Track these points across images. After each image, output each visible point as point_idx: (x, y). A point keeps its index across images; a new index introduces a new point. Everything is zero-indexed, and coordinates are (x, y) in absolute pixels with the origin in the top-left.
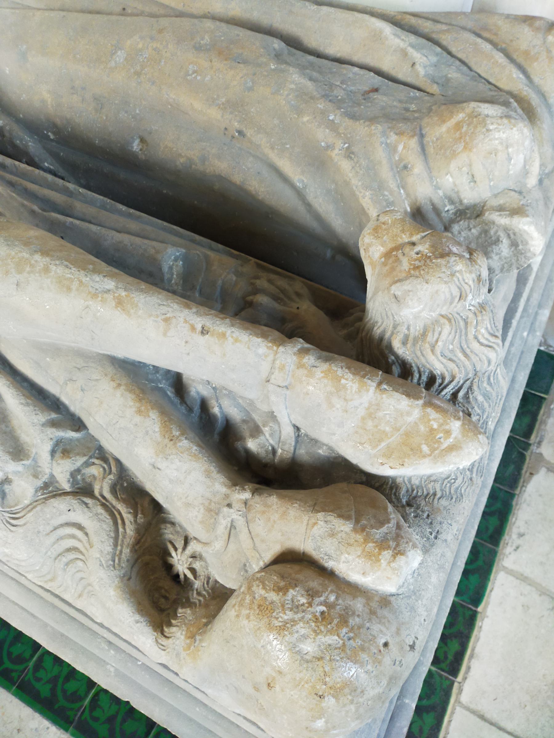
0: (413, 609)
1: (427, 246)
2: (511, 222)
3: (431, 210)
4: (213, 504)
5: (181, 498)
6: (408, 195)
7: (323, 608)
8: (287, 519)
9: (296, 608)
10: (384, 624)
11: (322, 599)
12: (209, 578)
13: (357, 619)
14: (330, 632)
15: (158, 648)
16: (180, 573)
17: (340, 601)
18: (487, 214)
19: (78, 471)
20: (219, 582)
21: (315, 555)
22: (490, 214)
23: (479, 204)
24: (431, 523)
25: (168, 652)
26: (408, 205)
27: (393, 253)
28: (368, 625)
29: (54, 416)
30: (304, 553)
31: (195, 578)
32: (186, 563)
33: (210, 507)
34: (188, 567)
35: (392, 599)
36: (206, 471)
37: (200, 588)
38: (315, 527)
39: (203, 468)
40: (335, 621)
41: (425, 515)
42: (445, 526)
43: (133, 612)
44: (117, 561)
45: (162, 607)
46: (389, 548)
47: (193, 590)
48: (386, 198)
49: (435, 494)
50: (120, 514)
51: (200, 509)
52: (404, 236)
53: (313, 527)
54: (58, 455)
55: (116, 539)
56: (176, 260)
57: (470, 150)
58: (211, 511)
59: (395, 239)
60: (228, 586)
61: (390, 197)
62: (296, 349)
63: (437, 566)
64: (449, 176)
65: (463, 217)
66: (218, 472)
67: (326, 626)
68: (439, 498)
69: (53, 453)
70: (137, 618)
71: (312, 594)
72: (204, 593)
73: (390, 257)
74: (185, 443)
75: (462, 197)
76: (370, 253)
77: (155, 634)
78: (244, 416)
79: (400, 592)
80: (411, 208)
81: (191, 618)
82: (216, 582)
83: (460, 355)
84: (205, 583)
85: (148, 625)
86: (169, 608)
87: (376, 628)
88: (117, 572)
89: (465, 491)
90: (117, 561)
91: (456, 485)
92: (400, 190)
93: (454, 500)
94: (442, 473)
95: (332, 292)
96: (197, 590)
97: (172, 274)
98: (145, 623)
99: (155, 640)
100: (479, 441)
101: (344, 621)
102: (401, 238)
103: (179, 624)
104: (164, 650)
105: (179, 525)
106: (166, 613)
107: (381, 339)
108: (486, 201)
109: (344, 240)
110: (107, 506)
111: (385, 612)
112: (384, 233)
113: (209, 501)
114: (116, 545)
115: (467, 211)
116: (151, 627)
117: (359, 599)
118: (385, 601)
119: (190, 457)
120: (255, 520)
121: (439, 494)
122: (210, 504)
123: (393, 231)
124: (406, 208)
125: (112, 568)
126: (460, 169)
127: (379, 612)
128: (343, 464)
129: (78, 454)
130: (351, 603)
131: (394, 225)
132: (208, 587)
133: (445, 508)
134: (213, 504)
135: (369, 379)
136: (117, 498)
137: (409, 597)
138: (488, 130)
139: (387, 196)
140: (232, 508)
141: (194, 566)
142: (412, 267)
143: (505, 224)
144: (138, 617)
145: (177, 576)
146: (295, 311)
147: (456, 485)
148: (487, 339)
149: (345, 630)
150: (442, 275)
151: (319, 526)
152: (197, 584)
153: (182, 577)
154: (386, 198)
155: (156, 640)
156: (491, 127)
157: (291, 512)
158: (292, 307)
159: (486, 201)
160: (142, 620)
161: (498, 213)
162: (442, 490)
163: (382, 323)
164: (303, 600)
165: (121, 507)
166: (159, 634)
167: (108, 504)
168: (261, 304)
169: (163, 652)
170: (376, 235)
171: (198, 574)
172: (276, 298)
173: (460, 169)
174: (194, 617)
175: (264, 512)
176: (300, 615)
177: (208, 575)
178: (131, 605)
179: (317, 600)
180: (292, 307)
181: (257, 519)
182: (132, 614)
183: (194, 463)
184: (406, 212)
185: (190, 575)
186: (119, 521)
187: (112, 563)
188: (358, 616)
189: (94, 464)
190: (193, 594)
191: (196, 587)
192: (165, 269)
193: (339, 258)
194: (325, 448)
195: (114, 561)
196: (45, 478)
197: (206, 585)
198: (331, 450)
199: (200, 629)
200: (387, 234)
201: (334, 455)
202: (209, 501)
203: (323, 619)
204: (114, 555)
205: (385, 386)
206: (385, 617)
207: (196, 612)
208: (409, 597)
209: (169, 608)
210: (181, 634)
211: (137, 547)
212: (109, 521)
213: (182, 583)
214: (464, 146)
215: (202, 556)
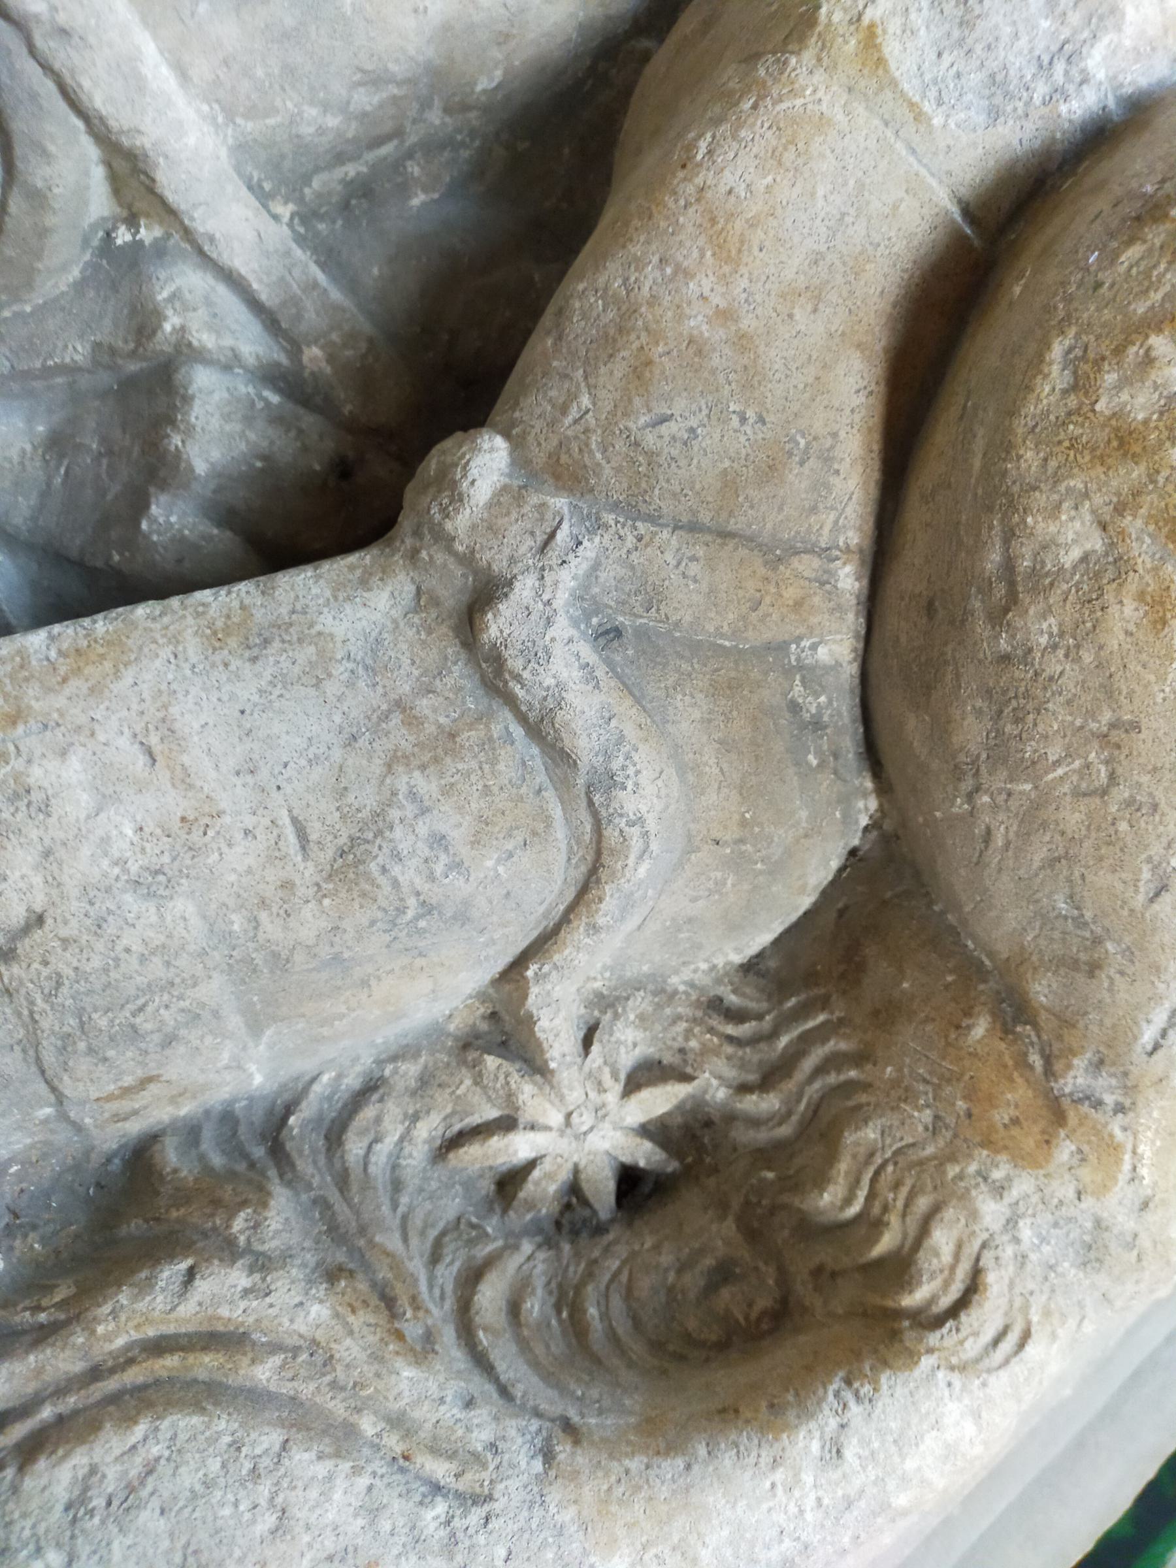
4: (424, 704)
5: (287, 885)
8: (753, 224)
12: (716, 1005)
15: (1003, 1374)
16: (626, 1159)
20: (760, 955)
21: (1014, 135)
25: (1047, 1313)
30: (967, 211)
31: (687, 1078)
32: (601, 1089)
33: (430, 729)
34: (619, 1088)
36: (215, 638)
37: (743, 1065)
38: (891, 48)
43: (775, 1463)
44: (440, 1470)
45: (763, 1302)
47: (731, 1118)
50: (159, 1347)
51: (413, 795)
53: (881, 62)
58: (452, 736)
60: (806, 902)
70: (815, 1446)
72: (784, 1041)
77: (927, 1362)
78: (29, 421)
81: (927, 1116)
82: (750, 967)
84: (730, 1030)
85: (866, 1389)
86: (782, 1271)
90: (440, 1470)
96: (744, 1089)
98: (855, 1409)
99: (956, 1378)
103: (923, 1203)
104: (1026, 1336)
105: (394, 1058)
106: (803, 1289)
110: (60, 1420)
113: (396, 719)
114: (341, 1439)
116: (884, 1378)
119: (76, 685)
120: (651, 455)
122: (413, 721)
125: (476, 1516)
128: (522, 146)
132: (760, 1017)
134: (424, 704)
140: (510, 583)
141: (627, 1060)
144: (806, 1441)
145: (629, 1179)
151: (894, 26)
152: (713, 1085)
153: (644, 1154)
155: (962, 1368)
157: (729, 178)
160: (833, 1423)
166: (933, 1338)
167: (47, 1413)
169: (1030, 1349)
171: (668, 1058)
174: (925, 1094)
175: (641, 371)
177: (698, 1004)
181: (649, 439)
182: (779, 1476)
183: (129, 676)
186: (206, 1364)
187: (441, 1507)
190: (755, 1122)
191: (721, 1094)
194: (414, 169)
195: (437, 1489)
197: (745, 1030)
198: (442, 147)
199: (1023, 1063)
201: (465, 154)
207: (895, 1083)
209: (782, 1271)
210: (999, 1190)
213: (673, 1166)
215: (600, 996)
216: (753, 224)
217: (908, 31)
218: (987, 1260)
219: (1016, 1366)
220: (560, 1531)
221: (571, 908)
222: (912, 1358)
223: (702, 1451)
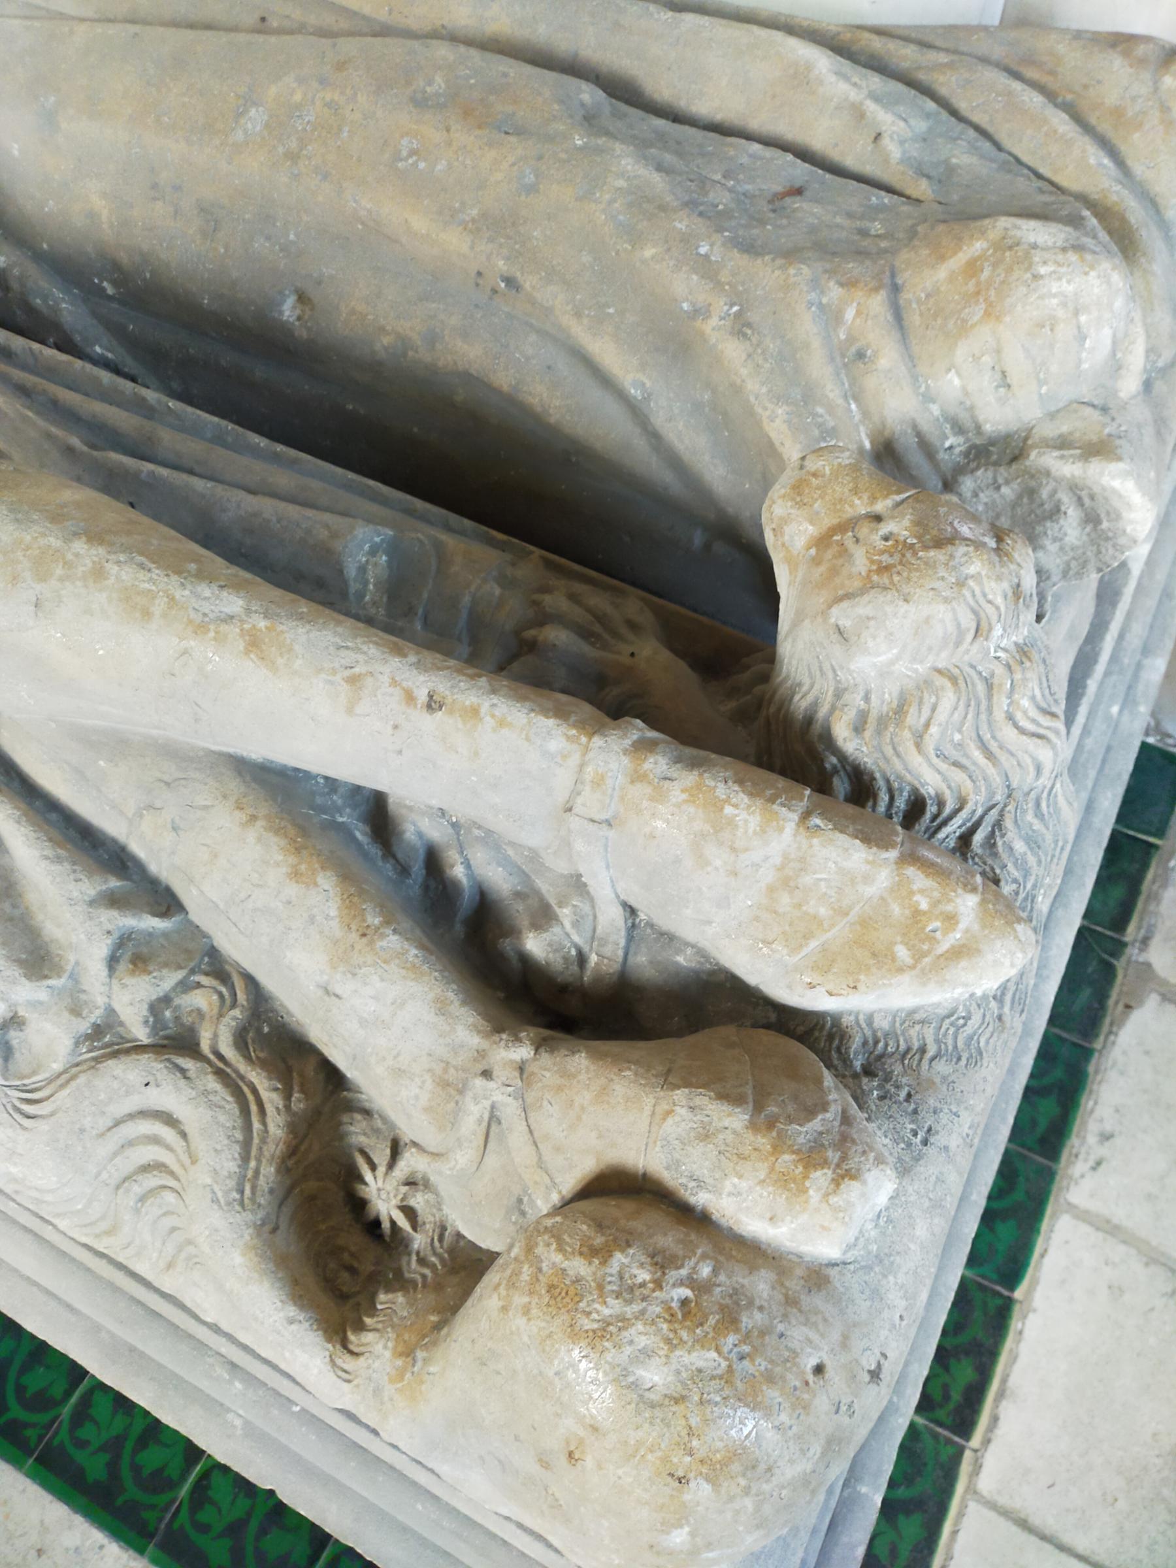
0: (876, 1294)
1: (906, 522)
2: (1085, 472)
3: (915, 445)
4: (452, 1071)
5: (384, 1059)
6: (866, 414)
7: (686, 1292)
8: (608, 1103)
9: (628, 1291)
10: (815, 1325)
11: (684, 1272)
12: (443, 1228)
13: (758, 1316)
14: (701, 1343)
15: (335, 1378)
16: (381, 1218)
17: (722, 1278)
18: (1033, 454)
19: (166, 1000)
20: (464, 1237)
21: (669, 1178)
22: (1040, 454)
23: (1016, 432)
24: (915, 1112)
25: (357, 1386)
26: (867, 435)
27: (835, 538)
28: (781, 1327)
29: (114, 883)
30: (644, 1175)
31: (415, 1228)
32: (395, 1196)
33: (446, 1077)
35: (833, 1272)
36: (437, 1000)
37: (425, 1249)
38: (670, 1121)
39: (431, 995)
40: (712, 1320)
41: (903, 1094)
42: (944, 1117)
43: (282, 1301)
45: (345, 1289)
46: (825, 1163)
48: (820, 420)
49: (923, 1050)
50: (255, 1091)
51: (424, 1082)
52: (857, 502)
53: (664, 1119)
54: (123, 966)
55: (246, 1144)
56: (373, 552)
57: (998, 318)
58: (448, 1085)
59: (838, 507)
61: (828, 418)
62: (627, 742)
63: (927, 1204)
64: (952, 373)
65: (983, 461)
66: (464, 1003)
67: (691, 1330)
68: (933, 1059)
69: (112, 962)
70: (292, 1314)
71: (662, 1262)
72: (433, 1259)
73: (828, 546)
74: (392, 941)
75: (981, 418)
76: (786, 538)
77: (330, 1346)
78: (519, 884)
79: (849, 1257)
80: (872, 443)
81: (405, 1314)
82: (459, 1236)
83: (977, 755)
84: (436, 1238)
86: (359, 1292)
87: (797, 1333)
88: (248, 1216)
89: (987, 1042)
91: (969, 1030)
92: (849, 404)
93: (963, 1062)
94: (938, 1005)
95: (705, 620)
96: (418, 1253)
97: (366, 583)
98: (307, 1324)
99: (328, 1359)
100: (1016, 937)
101: (730, 1319)
102: (851, 506)
103: (380, 1326)
104: (349, 1381)
105: (380, 1116)
106: (352, 1301)
107: (809, 720)
108: (1033, 428)
109: (730, 510)
110: (228, 1074)
111: (817, 1300)
112: (816, 496)
113: (443, 1065)
114: (245, 1158)
115: (991, 448)
116: (320, 1333)
117: (763, 1272)
118: (818, 1277)
120: (541, 1106)
121: (932, 1050)
122: (445, 1071)
123: (834, 490)
124: (861, 441)
125: (238, 1208)
126: (976, 359)
127: (805, 1300)
128: (728, 985)
129: (166, 965)
130: (745, 1282)
131: (837, 479)
132: (442, 1247)
133: (944, 1078)
134: (452, 1071)
135: (783, 805)
136: (248, 1058)
137: (869, 1268)
138: (1036, 277)
139: (822, 416)
140: (492, 1079)
141: (412, 1202)
142: (874, 567)
143: (1073, 476)
144: (292, 1311)
145: (377, 1223)
146: (627, 660)
147: (969, 1030)
148: (1033, 721)
149: (732, 1339)
150: (938, 584)
151: (677, 1119)
152: (419, 1241)
153: (386, 1225)
154: (820, 420)
155: (332, 1361)
156: (1043, 270)
158: (619, 653)
159: (1033, 428)
161: (1056, 453)
162: (938, 1041)
163: (812, 686)
164: (644, 1276)
165: (257, 1077)
166: (338, 1346)
167: (228, 1070)
168: (554, 645)
169: (346, 1385)
170: (798, 499)
171: (420, 1219)
172: (586, 634)
173: (976, 359)
174: (411, 1311)
175: (560, 1089)
176: (636, 1307)
177: (441, 1221)
178: (278, 1285)
179: (673, 1275)
180: (619, 653)
181: (545, 1103)
182: (279, 1304)
183: (412, 984)
184: (861, 450)
185: (403, 1222)
186: (254, 1108)
188: (761, 1308)
189: (199, 985)
190: (409, 1263)
191: (416, 1246)
192: (351, 571)
193: (719, 548)
194: (689, 951)
196: (96, 1016)
197: (436, 1243)
198: (703, 957)
199: (424, 1336)
200: (822, 497)
201: (708, 966)
202: (443, 1065)
203: (687, 1315)
204: (242, 1180)
205: (817, 821)
206: (817, 1312)
208: (869, 1268)
209: (359, 1292)
210: (385, 1347)
211: (290, 1163)
212: (232, 1106)
214: (986, 311)
215: (428, 1180)
216: (608, 1103)
217: (677, 1124)
218: (367, 1355)
219: (339, 1381)
220: (242, 1236)
221: (432, 1154)
222: (329, 1340)
223: (280, 1275)
